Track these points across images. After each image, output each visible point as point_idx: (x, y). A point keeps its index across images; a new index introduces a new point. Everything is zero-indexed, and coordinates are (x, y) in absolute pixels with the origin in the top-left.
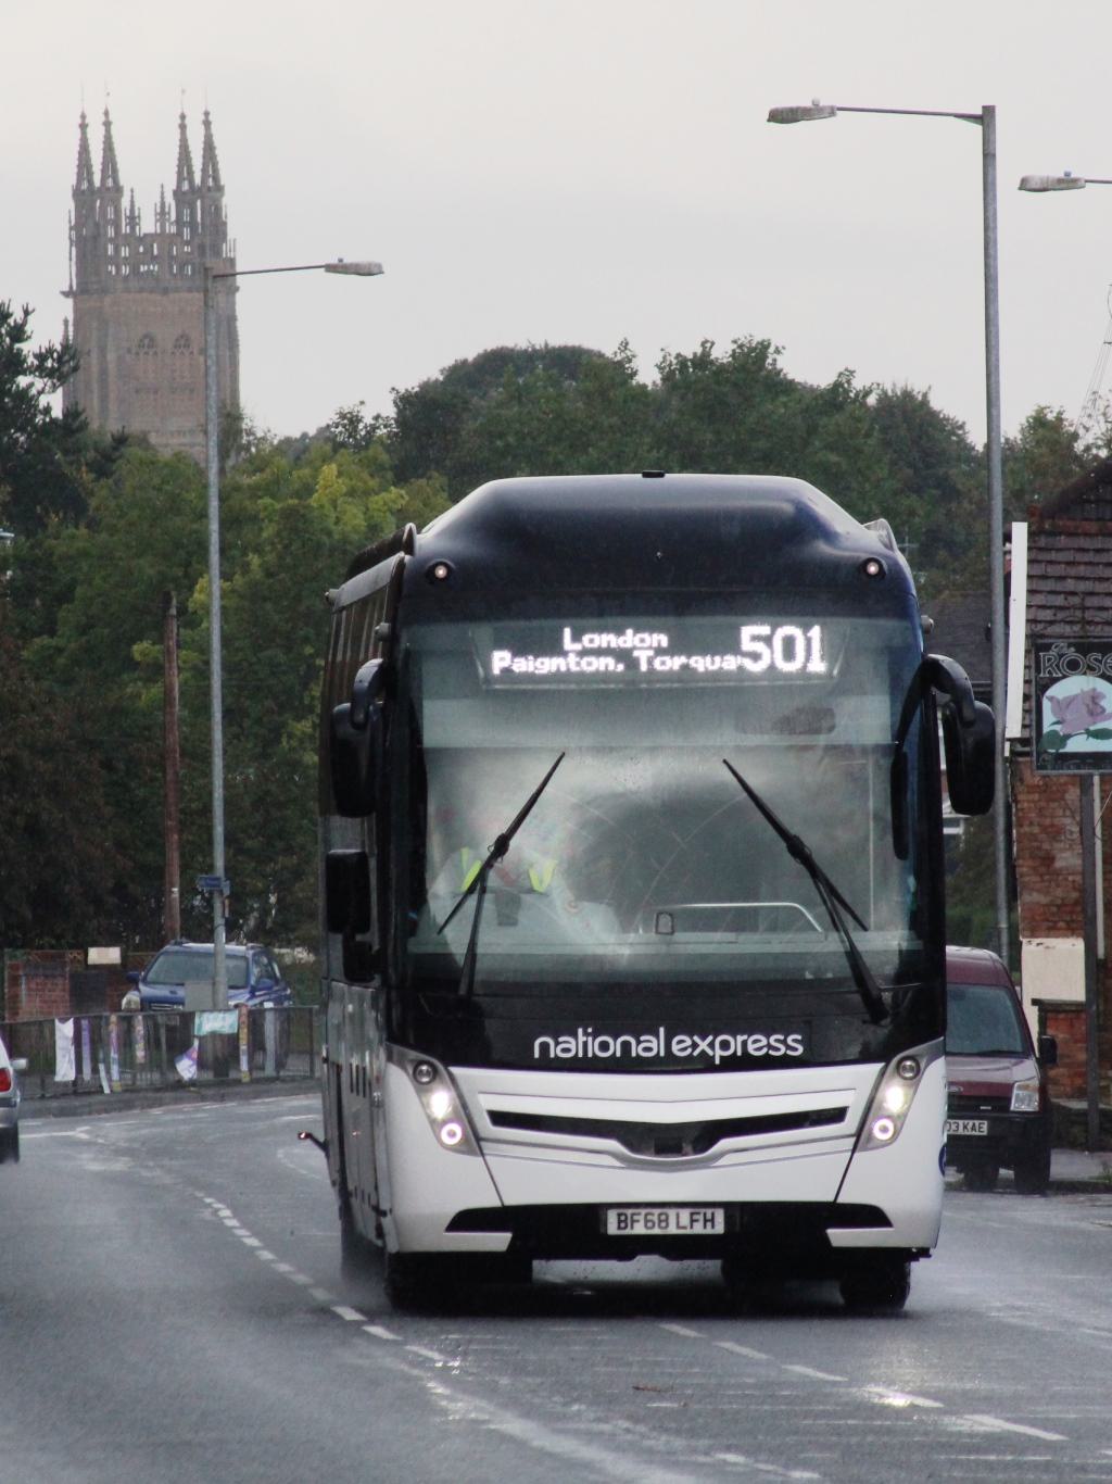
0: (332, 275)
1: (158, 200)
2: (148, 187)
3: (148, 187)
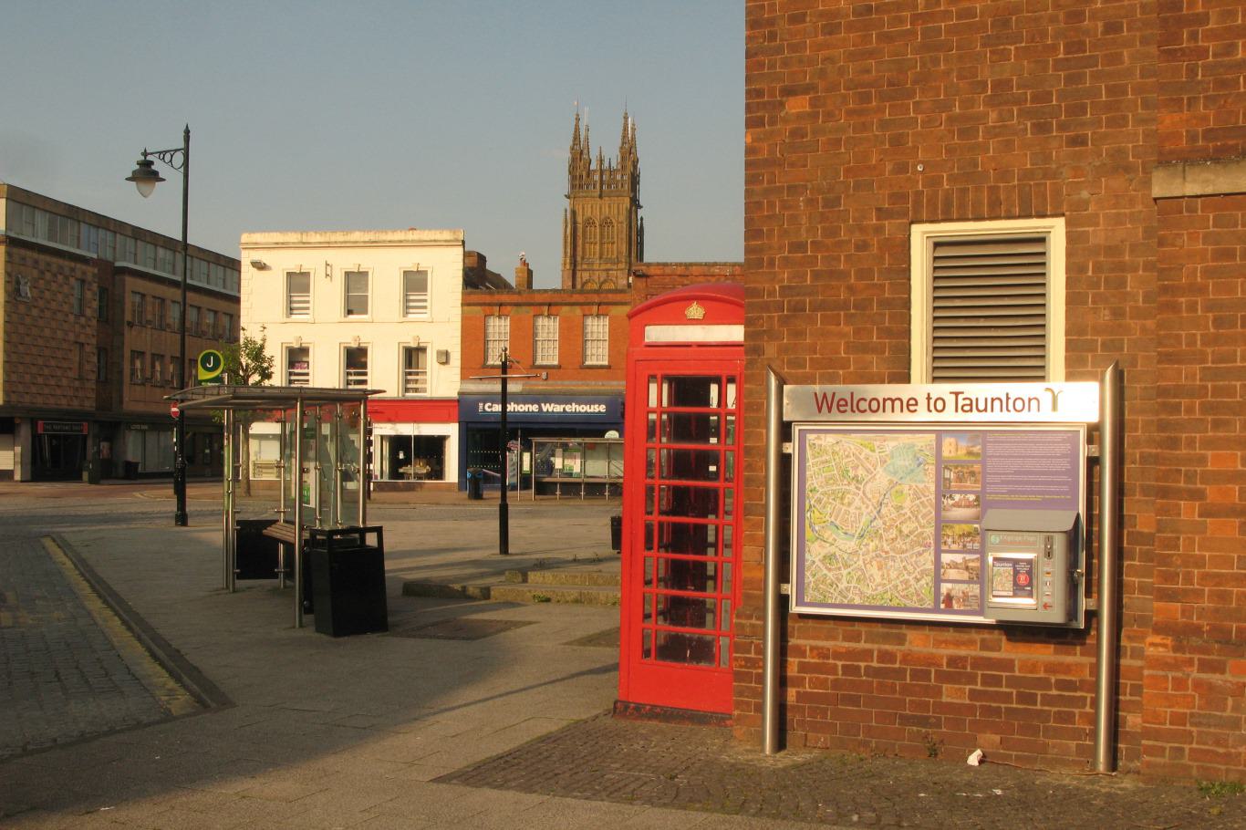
0: (182, 134)
1: (598, 154)
2: (605, 149)
3: (605, 149)
